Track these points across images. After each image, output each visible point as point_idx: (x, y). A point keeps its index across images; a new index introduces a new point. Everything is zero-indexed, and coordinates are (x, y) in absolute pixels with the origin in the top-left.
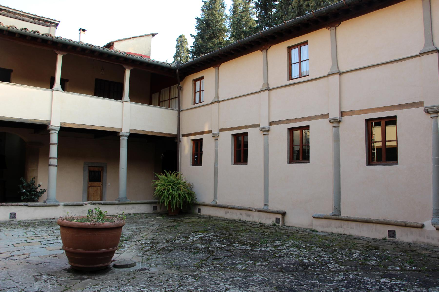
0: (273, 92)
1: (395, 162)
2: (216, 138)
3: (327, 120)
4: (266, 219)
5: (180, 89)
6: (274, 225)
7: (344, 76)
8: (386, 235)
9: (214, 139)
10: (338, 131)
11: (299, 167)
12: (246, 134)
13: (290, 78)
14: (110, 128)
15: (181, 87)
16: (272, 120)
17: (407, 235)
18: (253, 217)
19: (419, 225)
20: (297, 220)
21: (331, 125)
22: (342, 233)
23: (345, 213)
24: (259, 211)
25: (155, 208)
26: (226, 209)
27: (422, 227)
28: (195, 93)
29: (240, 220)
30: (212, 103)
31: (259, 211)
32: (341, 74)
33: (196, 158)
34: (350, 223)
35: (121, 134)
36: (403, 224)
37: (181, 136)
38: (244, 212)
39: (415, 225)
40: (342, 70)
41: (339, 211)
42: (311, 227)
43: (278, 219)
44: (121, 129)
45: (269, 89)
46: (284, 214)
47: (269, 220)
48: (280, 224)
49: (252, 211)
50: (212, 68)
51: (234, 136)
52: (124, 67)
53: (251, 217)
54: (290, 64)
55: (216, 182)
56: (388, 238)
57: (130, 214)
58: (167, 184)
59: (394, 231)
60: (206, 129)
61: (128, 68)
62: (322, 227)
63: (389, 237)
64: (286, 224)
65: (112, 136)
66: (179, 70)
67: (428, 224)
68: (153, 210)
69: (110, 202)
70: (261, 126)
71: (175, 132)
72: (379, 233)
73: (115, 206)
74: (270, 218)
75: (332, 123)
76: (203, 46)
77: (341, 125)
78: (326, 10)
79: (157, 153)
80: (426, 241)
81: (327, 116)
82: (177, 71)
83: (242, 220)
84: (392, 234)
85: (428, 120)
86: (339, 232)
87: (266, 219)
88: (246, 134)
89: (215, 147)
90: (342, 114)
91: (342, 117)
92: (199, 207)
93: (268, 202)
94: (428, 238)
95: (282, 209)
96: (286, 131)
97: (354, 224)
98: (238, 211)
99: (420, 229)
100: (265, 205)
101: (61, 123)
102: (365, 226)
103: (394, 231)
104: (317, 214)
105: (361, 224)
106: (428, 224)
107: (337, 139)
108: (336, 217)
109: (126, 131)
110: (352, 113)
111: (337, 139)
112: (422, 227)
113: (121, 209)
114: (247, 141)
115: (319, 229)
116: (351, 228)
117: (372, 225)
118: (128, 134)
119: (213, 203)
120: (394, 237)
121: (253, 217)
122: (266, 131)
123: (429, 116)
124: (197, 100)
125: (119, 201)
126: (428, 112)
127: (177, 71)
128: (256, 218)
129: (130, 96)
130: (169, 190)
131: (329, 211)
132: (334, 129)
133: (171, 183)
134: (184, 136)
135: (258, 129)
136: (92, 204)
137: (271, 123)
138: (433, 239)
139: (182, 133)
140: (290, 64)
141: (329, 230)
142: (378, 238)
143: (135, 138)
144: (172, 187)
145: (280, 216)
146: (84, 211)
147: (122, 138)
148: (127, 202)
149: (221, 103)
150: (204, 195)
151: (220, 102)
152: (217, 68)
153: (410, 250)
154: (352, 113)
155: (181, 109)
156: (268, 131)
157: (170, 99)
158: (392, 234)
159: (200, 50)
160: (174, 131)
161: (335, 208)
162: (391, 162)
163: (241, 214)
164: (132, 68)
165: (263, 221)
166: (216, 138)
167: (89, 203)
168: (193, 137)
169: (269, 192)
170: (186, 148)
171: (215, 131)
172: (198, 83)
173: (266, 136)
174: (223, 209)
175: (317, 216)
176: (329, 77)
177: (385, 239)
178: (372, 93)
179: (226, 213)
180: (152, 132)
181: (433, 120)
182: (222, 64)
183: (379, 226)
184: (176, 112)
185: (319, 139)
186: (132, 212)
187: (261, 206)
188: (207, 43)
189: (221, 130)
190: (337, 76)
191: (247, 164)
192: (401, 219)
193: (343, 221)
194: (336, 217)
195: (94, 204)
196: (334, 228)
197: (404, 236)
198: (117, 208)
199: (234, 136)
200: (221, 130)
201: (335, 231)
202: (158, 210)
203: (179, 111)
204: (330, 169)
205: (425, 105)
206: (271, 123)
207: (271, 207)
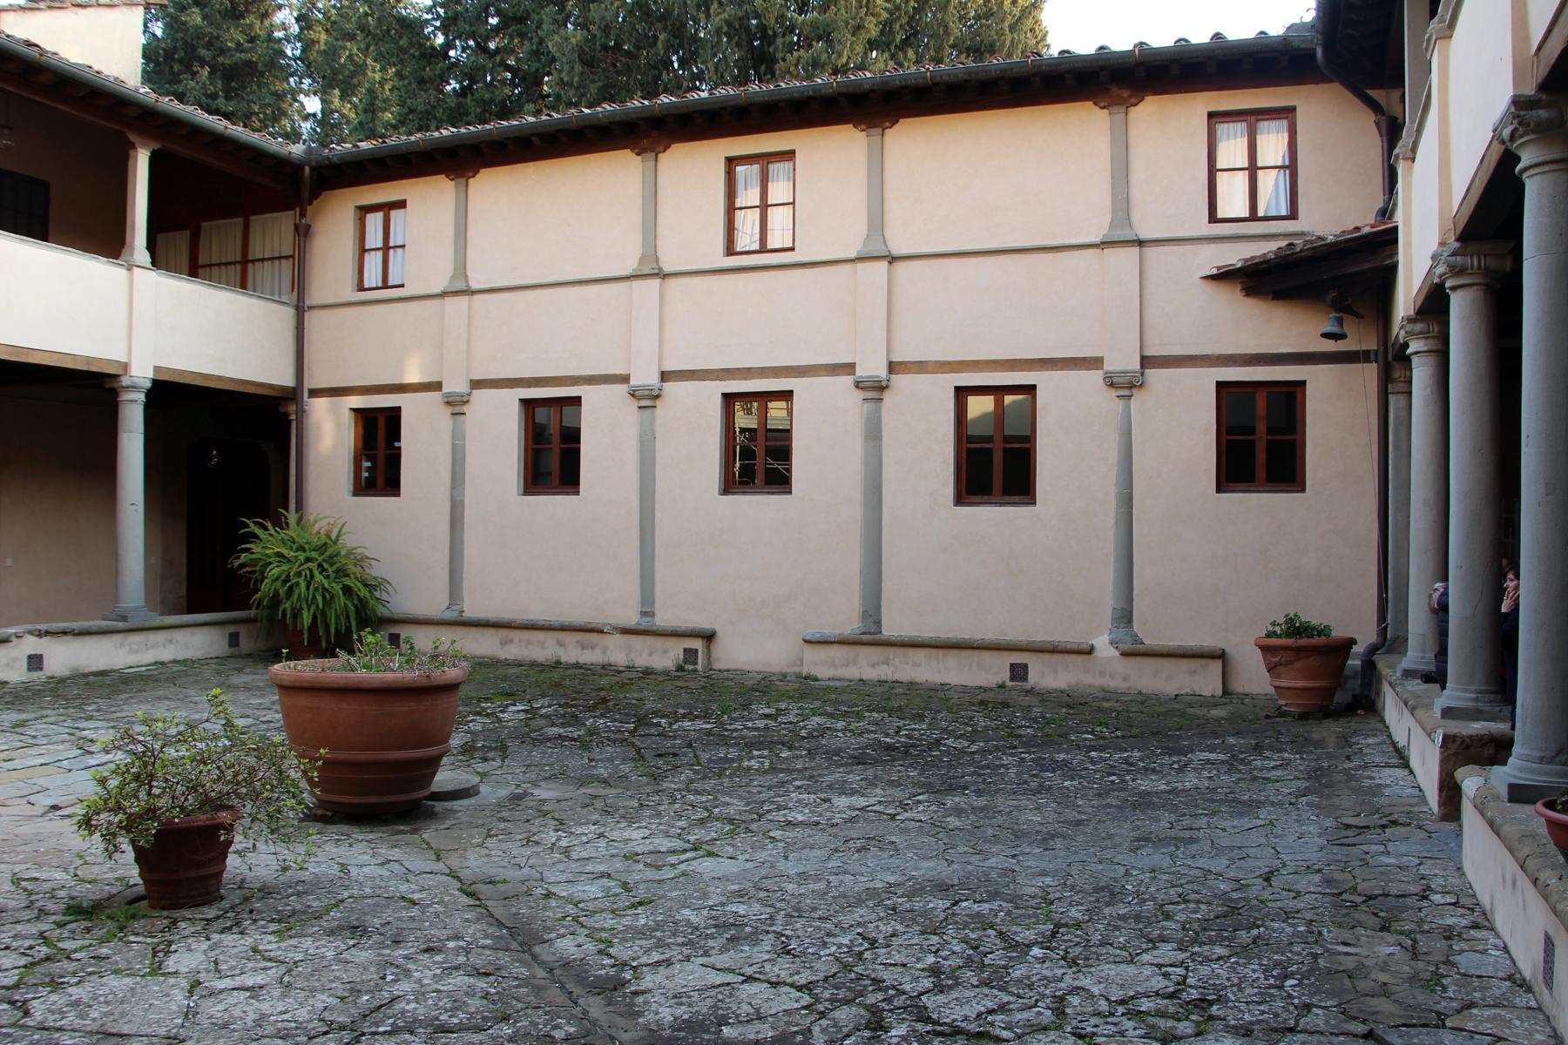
0: (673, 283)
1: (1026, 499)
2: (458, 409)
3: (848, 380)
4: (650, 655)
5: (303, 233)
6: (680, 669)
7: (899, 266)
8: (1005, 675)
9: (449, 410)
10: (879, 410)
11: (757, 506)
12: (577, 401)
13: (730, 251)
14: (89, 359)
15: (309, 227)
16: (670, 366)
17: (1056, 672)
18: (604, 651)
19: (1084, 647)
20: (749, 649)
21: (859, 395)
22: (890, 678)
23: (890, 630)
24: (626, 631)
25: (234, 640)
26: (503, 633)
27: (1090, 651)
28: (363, 251)
29: (558, 663)
30: (443, 295)
31: (626, 631)
32: (893, 259)
33: (368, 469)
34: (910, 651)
35: (125, 381)
36: (1049, 646)
37: (306, 394)
38: (571, 638)
39: (1075, 647)
40: (896, 252)
41: (878, 623)
42: (796, 669)
43: (690, 654)
44: (126, 366)
45: (663, 276)
46: (709, 637)
47: (664, 657)
48: (699, 667)
49: (601, 632)
50: (442, 177)
51: (528, 405)
52: (132, 138)
53: (598, 651)
54: (731, 209)
55: (451, 548)
56: (1009, 684)
57: (162, 663)
58: (302, 556)
59: (1026, 666)
60: (412, 376)
61: (144, 146)
62: (826, 666)
63: (1012, 679)
64: (717, 666)
65: (82, 393)
66: (312, 169)
67: (1102, 642)
68: (231, 645)
69: (91, 623)
70: (633, 382)
71: (286, 379)
72: (989, 672)
73: (117, 638)
74: (665, 652)
75: (862, 388)
76: (205, 35)
77: (887, 395)
78: (1275, 253)
79: (226, 448)
80: (1098, 681)
81: (849, 368)
82: (307, 170)
83: (563, 660)
84: (1019, 672)
85: (1109, 401)
86: (883, 678)
87: (650, 655)
88: (577, 401)
89: (454, 438)
90: (893, 367)
91: (893, 377)
92: (395, 630)
93: (653, 602)
94: (1102, 674)
95: (704, 624)
96: (718, 400)
97: (920, 654)
98: (550, 634)
99: (1086, 657)
100: (644, 614)
101: (157, 369)
102: (952, 658)
103: (1026, 666)
104: (814, 632)
105: (941, 652)
106: (1102, 642)
107: (874, 433)
108: (871, 638)
109: (142, 372)
110: (920, 367)
111: (874, 433)
112: (1090, 651)
113: (134, 647)
114: (579, 430)
115: (823, 672)
116: (915, 665)
117: (969, 653)
118: (148, 384)
119: (449, 615)
120: (1025, 679)
121: (604, 651)
122: (647, 399)
123: (1113, 393)
124: (372, 276)
125: (124, 618)
126: (1112, 385)
127: (307, 170)
128: (617, 652)
129: (151, 247)
130: (312, 576)
131: (849, 623)
132: (866, 405)
133: (314, 555)
134: (315, 393)
135: (622, 389)
136: (40, 634)
137: (665, 376)
138: (1113, 678)
139: (310, 383)
140: (731, 209)
141: (853, 673)
142: (984, 684)
143: (173, 399)
144: (320, 565)
145: (697, 644)
146: (14, 660)
147: (125, 396)
148: (147, 624)
149: (477, 297)
150: (415, 589)
151: (474, 292)
152: (463, 180)
153: (1071, 702)
154: (920, 367)
155: (308, 303)
156: (658, 397)
157: (245, 262)
158: (1019, 672)
159: (191, 48)
160: (281, 376)
161: (865, 615)
162: (1016, 499)
163: (561, 644)
164: (157, 146)
165: (642, 661)
166: (458, 409)
167: (31, 633)
168: (357, 401)
169: (658, 576)
170: (329, 434)
171: (456, 384)
172: (374, 221)
173: (649, 411)
174: (492, 631)
175: (817, 637)
176: (860, 266)
177: (1002, 686)
178: (980, 319)
179: (503, 643)
180: (220, 378)
181: (1121, 403)
182: (482, 171)
183: (987, 655)
184: (289, 312)
185: (821, 428)
186: (166, 655)
187: (632, 618)
188: (219, 27)
189: (477, 384)
190: (884, 265)
191: (1303, 490)
192: (1039, 636)
193: (892, 649)
194: (871, 638)
195: (47, 633)
196: (868, 667)
197: (1046, 676)
198: (122, 645)
199: (528, 405)
200: (477, 384)
201: (870, 674)
202: (246, 645)
203: (301, 310)
204: (854, 512)
205: (1107, 367)
206: (665, 376)
207: (663, 620)
